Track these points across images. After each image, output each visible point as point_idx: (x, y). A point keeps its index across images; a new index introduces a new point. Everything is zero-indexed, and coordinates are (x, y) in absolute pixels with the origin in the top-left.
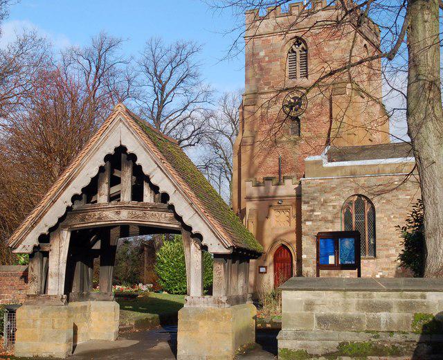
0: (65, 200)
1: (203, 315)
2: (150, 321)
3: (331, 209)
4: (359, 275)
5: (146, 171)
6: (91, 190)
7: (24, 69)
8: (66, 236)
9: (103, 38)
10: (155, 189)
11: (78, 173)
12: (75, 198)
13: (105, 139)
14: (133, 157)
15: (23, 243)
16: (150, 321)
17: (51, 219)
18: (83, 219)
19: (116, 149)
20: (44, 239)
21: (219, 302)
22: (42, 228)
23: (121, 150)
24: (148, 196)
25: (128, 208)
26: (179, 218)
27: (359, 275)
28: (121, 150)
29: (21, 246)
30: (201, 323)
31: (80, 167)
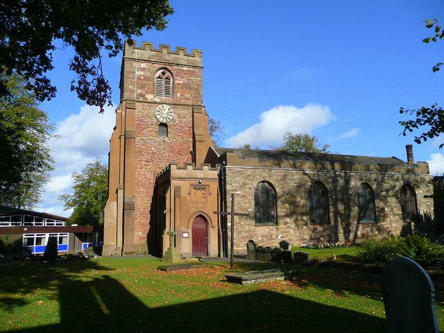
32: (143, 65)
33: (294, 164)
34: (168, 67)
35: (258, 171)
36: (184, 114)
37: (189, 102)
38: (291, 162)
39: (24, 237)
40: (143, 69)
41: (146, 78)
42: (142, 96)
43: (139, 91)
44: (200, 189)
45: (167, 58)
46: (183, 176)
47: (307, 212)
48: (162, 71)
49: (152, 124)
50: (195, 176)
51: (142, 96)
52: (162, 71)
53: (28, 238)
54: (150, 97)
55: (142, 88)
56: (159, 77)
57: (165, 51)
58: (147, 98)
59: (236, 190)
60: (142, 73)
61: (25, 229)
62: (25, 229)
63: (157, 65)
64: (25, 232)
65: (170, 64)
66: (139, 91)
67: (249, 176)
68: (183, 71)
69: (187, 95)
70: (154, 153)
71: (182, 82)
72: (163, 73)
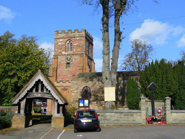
0: (25, 92)
1: (58, 118)
2: (107, 6)
3: (79, 90)
4: (89, 108)
5: (45, 85)
6: (31, 90)
7: (110, 94)
8: (25, 100)
9: (8, 33)
10: (47, 89)
11: (29, 86)
12: (28, 91)
13: (36, 78)
14: (42, 82)
15: (15, 101)
16: (107, 6)
17: (22, 96)
18: (29, 96)
19: (38, 80)
20: (20, 100)
21: (61, 115)
22: (20, 98)
23: (39, 80)
24: (45, 91)
25: (40, 93)
26: (53, 96)
27: (89, 108)
28: (39, 80)
29: (14, 102)
30: (57, 120)
31: (29, 84)
32: (61, 40)
33: (99, 79)
34: (71, 39)
35: (83, 83)
36: (76, 58)
37: (79, 53)
38: (98, 79)
39: (42, 108)
40: (61, 42)
41: (62, 45)
42: (61, 52)
43: (59, 51)
44: (65, 90)
45: (70, 35)
46: (58, 86)
47: (152, 102)
48: (69, 41)
49: (64, 64)
50: (63, 86)
51: (61, 52)
52: (69, 41)
53: (44, 109)
54: (64, 53)
55: (61, 50)
56: (68, 44)
57: (69, 33)
58: (62, 54)
59: (74, 91)
60: (61, 43)
61: (42, 105)
62: (42, 105)
63: (66, 39)
64: (43, 106)
65: (71, 38)
66: (59, 51)
67: (79, 85)
68: (77, 39)
69: (78, 50)
70: (64, 75)
71: (76, 45)
72: (70, 42)
